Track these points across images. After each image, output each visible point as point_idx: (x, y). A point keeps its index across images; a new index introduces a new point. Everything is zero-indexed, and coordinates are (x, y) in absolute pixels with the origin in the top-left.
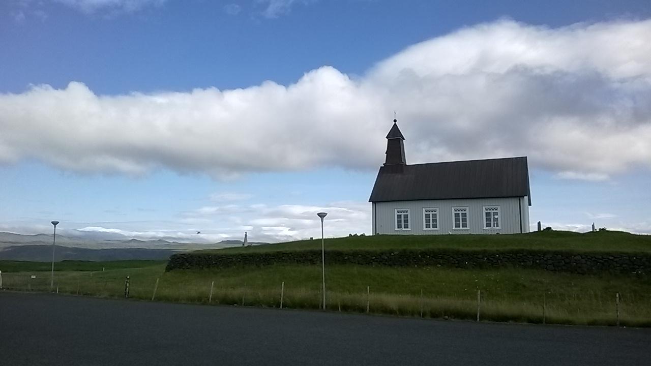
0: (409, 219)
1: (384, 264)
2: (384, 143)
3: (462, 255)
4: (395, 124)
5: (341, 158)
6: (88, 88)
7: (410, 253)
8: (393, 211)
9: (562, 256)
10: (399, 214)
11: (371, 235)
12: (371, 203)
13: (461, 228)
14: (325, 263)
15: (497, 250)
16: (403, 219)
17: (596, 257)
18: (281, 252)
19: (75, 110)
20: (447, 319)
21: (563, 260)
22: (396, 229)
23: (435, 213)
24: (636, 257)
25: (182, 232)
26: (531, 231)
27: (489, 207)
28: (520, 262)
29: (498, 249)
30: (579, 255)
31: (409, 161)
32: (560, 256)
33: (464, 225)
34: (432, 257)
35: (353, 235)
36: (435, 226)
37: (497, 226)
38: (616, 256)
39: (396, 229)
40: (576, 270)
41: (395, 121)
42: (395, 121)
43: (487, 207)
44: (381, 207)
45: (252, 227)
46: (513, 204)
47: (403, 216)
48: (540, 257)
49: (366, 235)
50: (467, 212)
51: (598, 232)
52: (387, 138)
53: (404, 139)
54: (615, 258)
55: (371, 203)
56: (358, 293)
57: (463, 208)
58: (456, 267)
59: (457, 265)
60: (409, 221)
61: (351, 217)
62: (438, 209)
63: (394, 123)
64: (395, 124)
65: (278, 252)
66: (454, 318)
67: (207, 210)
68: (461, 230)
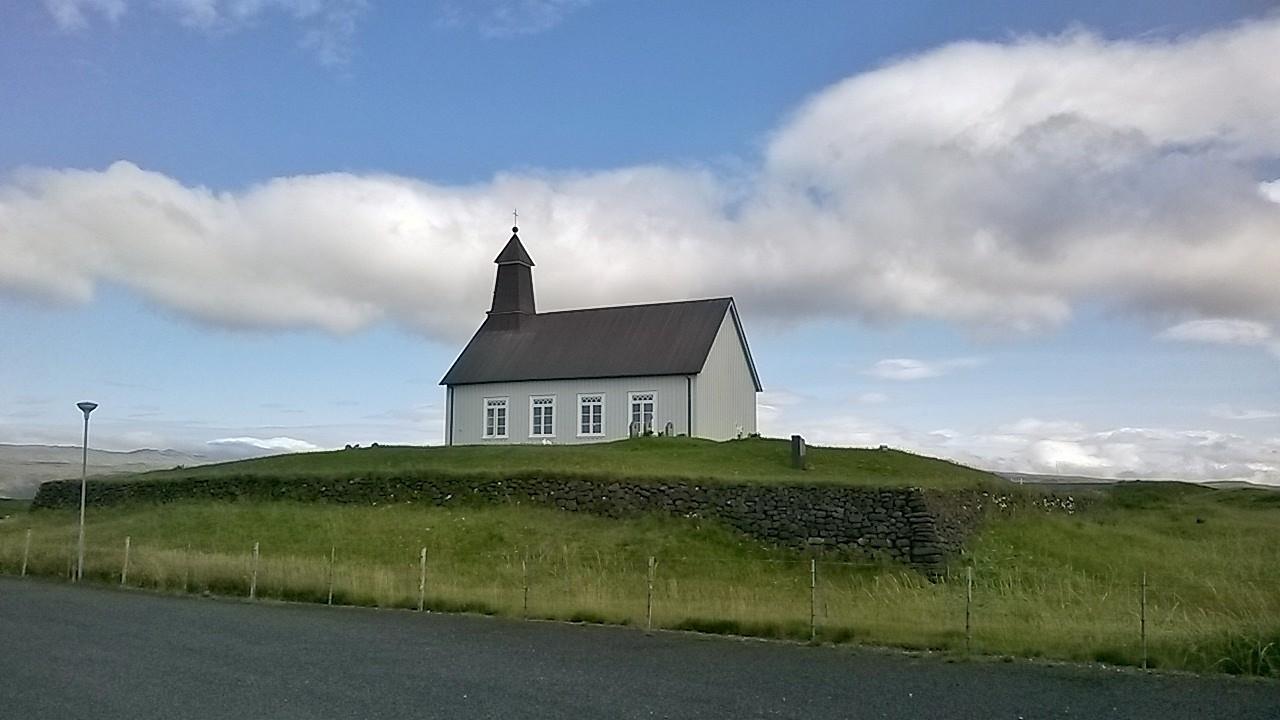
0: (507, 417)
1: (745, 487)
3: (450, 482)
4: (515, 236)
5: (398, 304)
7: (378, 479)
8: (481, 401)
9: (592, 484)
10: (584, 404)
11: (444, 444)
12: (446, 386)
13: (543, 435)
14: (86, 506)
15: (501, 473)
16: (642, 412)
17: (642, 487)
18: (193, 478)
19: (139, 208)
20: (207, 596)
21: (592, 490)
22: (580, 434)
23: (650, 402)
24: (700, 488)
26: (701, 432)
27: (587, 396)
28: (531, 495)
29: (503, 470)
30: (617, 482)
32: (589, 483)
33: (597, 430)
34: (409, 486)
35: (353, 446)
38: (672, 486)
39: (580, 434)
40: (607, 511)
41: (515, 230)
42: (515, 230)
43: (536, 398)
44: (463, 395)
46: (675, 388)
47: (642, 408)
48: (560, 484)
49: (762, 436)
51: (746, 439)
54: (670, 488)
55: (446, 386)
56: (227, 554)
57: (648, 394)
58: (438, 505)
59: (439, 501)
60: (506, 421)
61: (416, 417)
62: (603, 397)
63: (513, 233)
64: (515, 236)
65: (189, 479)
68: (592, 437)
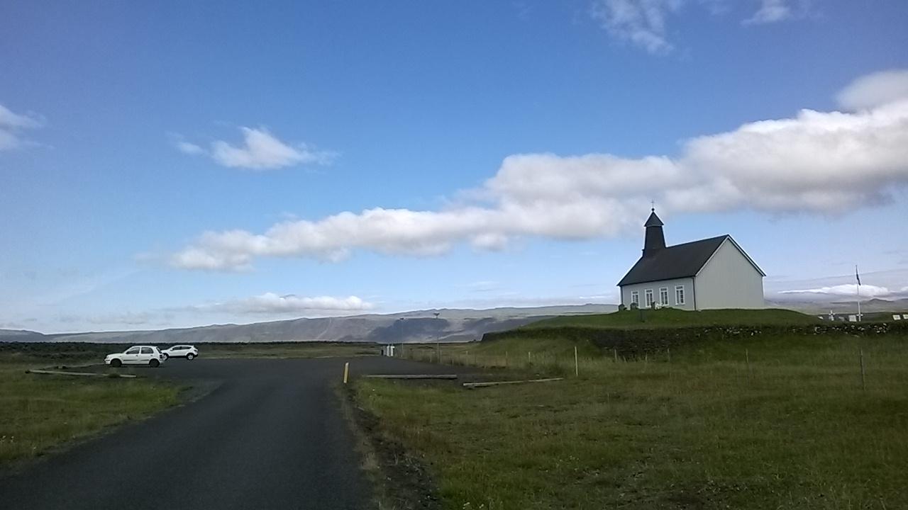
4: (653, 213)
8: (631, 292)
26: (700, 308)
31: (667, 246)
36: (666, 303)
42: (653, 210)
52: (645, 225)
62: (683, 286)
64: (653, 213)
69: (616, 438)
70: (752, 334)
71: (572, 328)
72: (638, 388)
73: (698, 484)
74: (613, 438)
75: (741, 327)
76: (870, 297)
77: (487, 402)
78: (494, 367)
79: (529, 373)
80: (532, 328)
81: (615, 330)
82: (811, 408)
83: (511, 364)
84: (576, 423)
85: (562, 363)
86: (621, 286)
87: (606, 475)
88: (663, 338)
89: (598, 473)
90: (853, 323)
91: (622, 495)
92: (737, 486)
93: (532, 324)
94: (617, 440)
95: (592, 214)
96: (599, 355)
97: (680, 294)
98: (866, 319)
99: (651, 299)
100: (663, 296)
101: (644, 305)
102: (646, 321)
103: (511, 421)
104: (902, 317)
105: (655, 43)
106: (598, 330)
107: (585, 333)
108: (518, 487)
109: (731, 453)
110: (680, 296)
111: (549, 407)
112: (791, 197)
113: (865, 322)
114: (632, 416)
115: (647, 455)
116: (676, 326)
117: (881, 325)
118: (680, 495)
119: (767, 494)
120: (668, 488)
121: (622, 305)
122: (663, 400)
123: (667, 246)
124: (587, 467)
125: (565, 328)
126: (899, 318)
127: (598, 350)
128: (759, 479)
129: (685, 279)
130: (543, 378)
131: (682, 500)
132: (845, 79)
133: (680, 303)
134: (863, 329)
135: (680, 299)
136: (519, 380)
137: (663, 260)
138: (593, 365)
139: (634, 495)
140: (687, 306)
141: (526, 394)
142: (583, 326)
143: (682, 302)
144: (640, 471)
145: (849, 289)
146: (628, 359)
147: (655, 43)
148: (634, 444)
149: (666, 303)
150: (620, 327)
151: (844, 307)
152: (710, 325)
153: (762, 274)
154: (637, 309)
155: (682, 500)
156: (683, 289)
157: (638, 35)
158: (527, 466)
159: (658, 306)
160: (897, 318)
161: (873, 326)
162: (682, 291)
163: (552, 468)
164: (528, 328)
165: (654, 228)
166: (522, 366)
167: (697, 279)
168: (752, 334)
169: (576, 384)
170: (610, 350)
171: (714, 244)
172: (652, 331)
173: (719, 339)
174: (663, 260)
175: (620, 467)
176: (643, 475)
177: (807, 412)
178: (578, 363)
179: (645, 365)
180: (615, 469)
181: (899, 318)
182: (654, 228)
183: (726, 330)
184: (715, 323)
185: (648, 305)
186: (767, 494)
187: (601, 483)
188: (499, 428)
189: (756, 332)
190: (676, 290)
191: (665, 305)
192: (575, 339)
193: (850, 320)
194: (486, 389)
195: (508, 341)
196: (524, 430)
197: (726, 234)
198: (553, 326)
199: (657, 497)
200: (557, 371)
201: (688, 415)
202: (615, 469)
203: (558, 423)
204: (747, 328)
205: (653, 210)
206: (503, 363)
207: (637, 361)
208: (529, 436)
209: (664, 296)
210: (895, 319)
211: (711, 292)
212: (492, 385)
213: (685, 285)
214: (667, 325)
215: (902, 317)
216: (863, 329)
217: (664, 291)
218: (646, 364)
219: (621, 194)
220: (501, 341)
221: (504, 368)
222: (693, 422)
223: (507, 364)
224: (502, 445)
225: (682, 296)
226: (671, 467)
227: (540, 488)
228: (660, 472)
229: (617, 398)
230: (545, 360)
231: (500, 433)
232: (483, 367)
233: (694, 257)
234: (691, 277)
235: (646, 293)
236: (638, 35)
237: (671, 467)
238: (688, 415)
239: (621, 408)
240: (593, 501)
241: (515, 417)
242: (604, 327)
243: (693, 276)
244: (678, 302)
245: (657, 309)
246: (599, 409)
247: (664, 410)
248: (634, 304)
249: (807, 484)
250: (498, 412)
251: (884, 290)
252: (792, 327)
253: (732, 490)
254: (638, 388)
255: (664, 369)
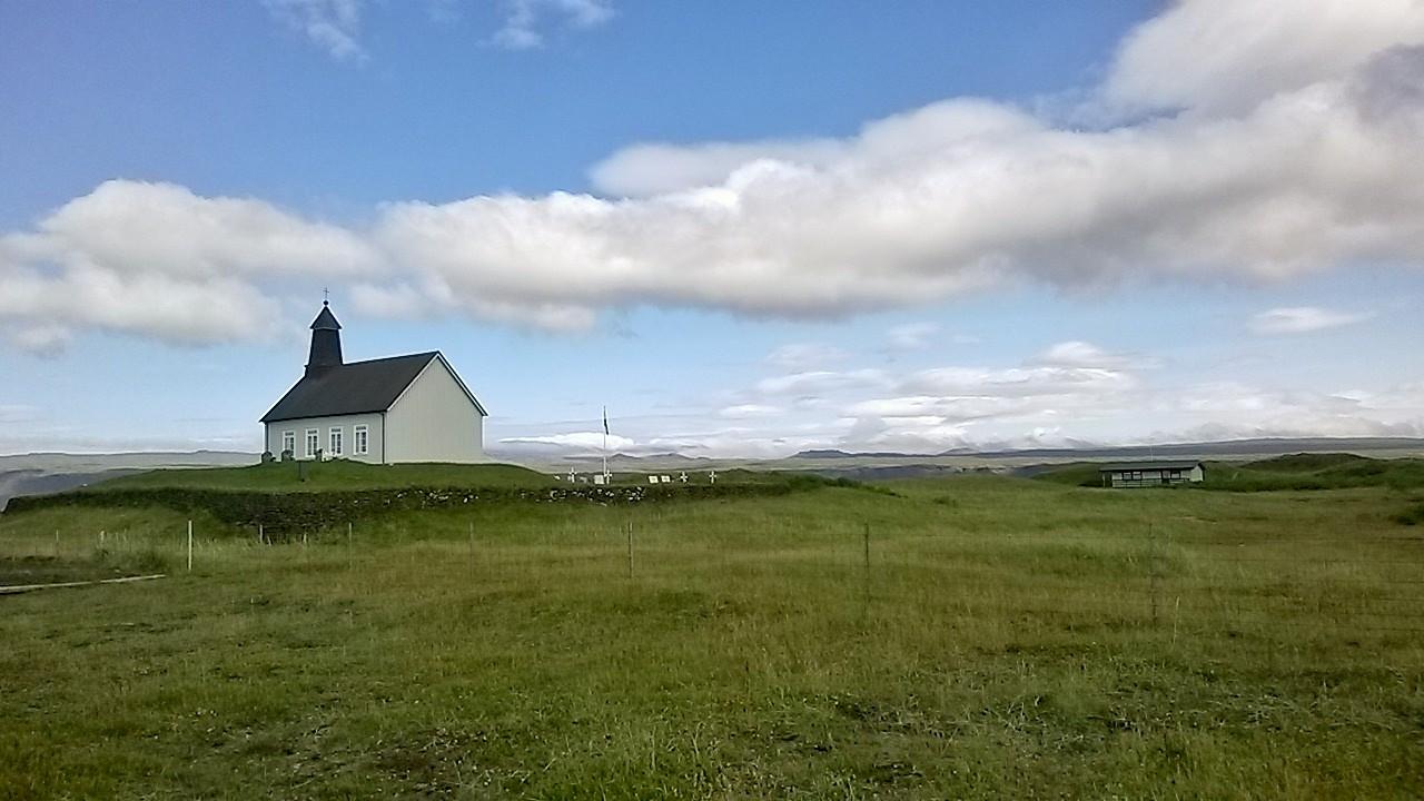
2: (308, 337)
4: (326, 308)
6: (146, 184)
8: (283, 432)
22: (355, 453)
25: (1042, 425)
26: (390, 461)
31: (344, 363)
36: (339, 452)
37: (364, 450)
39: (355, 453)
42: (326, 303)
45: (855, 419)
50: (341, 433)
52: (312, 327)
53: (340, 327)
62: (342, 428)
64: (326, 308)
66: (685, 592)
67: (772, 384)
69: (276, 671)
70: (466, 500)
71: (179, 490)
72: (299, 588)
73: (421, 737)
74: (269, 671)
75: (450, 490)
76: (611, 452)
77: (24, 621)
78: (31, 558)
79: (102, 567)
80: (104, 489)
81: (256, 494)
82: (568, 608)
83: (63, 553)
84: (200, 650)
85: (165, 549)
86: (267, 423)
87: (263, 735)
88: (334, 507)
89: (249, 733)
90: (599, 486)
91: (297, 766)
92: (482, 733)
93: (106, 482)
94: (275, 675)
95: (226, 305)
96: (226, 536)
97: (360, 438)
98: (617, 478)
99: (315, 445)
100: (337, 440)
101: (303, 454)
102: (308, 480)
103: (78, 652)
104: (660, 479)
105: (343, 45)
106: (226, 494)
107: (204, 499)
108: (108, 772)
109: (466, 682)
110: (360, 442)
111: (143, 625)
112: (522, 302)
113: (614, 485)
114: (294, 632)
115: (332, 695)
116: (354, 488)
117: (635, 490)
118: (395, 757)
119: (528, 741)
120: (372, 747)
121: (268, 454)
122: (341, 604)
123: (344, 363)
124: (230, 725)
125: (166, 490)
126: (656, 481)
127: (223, 527)
128: (511, 720)
129: (360, 416)
130: (128, 577)
131: (398, 765)
132: (606, 147)
133: (360, 452)
134: (612, 495)
135: (361, 445)
136: (82, 580)
137: (336, 382)
138: (218, 552)
139: (317, 765)
140: (371, 458)
141: (98, 605)
142: (199, 486)
143: (364, 450)
144: (323, 723)
145: (589, 439)
146: (274, 541)
147: (343, 45)
148: (307, 679)
149: (339, 452)
150: (263, 489)
151: (580, 464)
152: (407, 487)
153: (483, 413)
154: (292, 459)
155: (398, 765)
156: (317, 435)
157: (318, 29)
158: (121, 731)
159: (327, 455)
160: (653, 480)
161: (624, 490)
162: (364, 434)
163: (164, 730)
164: (98, 489)
165: (326, 333)
166: (86, 555)
167: (388, 416)
168: (466, 500)
169: (191, 583)
170: (245, 527)
171: (411, 367)
172: (316, 495)
173: (418, 508)
174: (336, 382)
175: (287, 720)
176: (329, 729)
177: (562, 613)
178: (193, 549)
179: (303, 549)
180: (279, 724)
181: (656, 481)
182: (326, 333)
183: (428, 494)
184: (413, 483)
185: (310, 454)
186: (528, 741)
187: (253, 750)
188: (56, 667)
189: (471, 497)
190: (284, 437)
191: (336, 455)
192: (184, 509)
193: (596, 482)
194: (22, 599)
195: (59, 512)
196: (105, 669)
197: (435, 350)
198: (144, 487)
199: (356, 765)
200: (153, 563)
201: (385, 626)
202: (279, 724)
203: (167, 652)
204: (459, 491)
205: (326, 303)
206: (49, 551)
207: (289, 542)
208: (116, 679)
209: (313, 442)
210: (652, 482)
211: (406, 437)
212: (30, 591)
213: (369, 424)
214: (340, 487)
215: (660, 479)
216: (612, 495)
217: (336, 433)
218: (304, 548)
219: (267, 280)
220: (44, 512)
221: (51, 558)
222: (395, 636)
223: (58, 552)
224: (63, 698)
225: (364, 442)
226: (375, 711)
227: (149, 770)
228: (358, 721)
229: (264, 604)
230: (129, 544)
231: (57, 677)
232: (9, 558)
233: (382, 384)
234: (379, 412)
235: (284, 437)
236: (318, 29)
237: (375, 711)
238: (385, 626)
239: (273, 620)
240: (247, 782)
241: (86, 644)
242: (235, 489)
243: (383, 411)
244: (357, 451)
245: (326, 462)
246: (240, 624)
247: (347, 621)
248: (287, 452)
249: (583, 723)
250: (48, 637)
251: (629, 443)
252: (520, 491)
253: (476, 741)
254: (299, 588)
255: (336, 555)
